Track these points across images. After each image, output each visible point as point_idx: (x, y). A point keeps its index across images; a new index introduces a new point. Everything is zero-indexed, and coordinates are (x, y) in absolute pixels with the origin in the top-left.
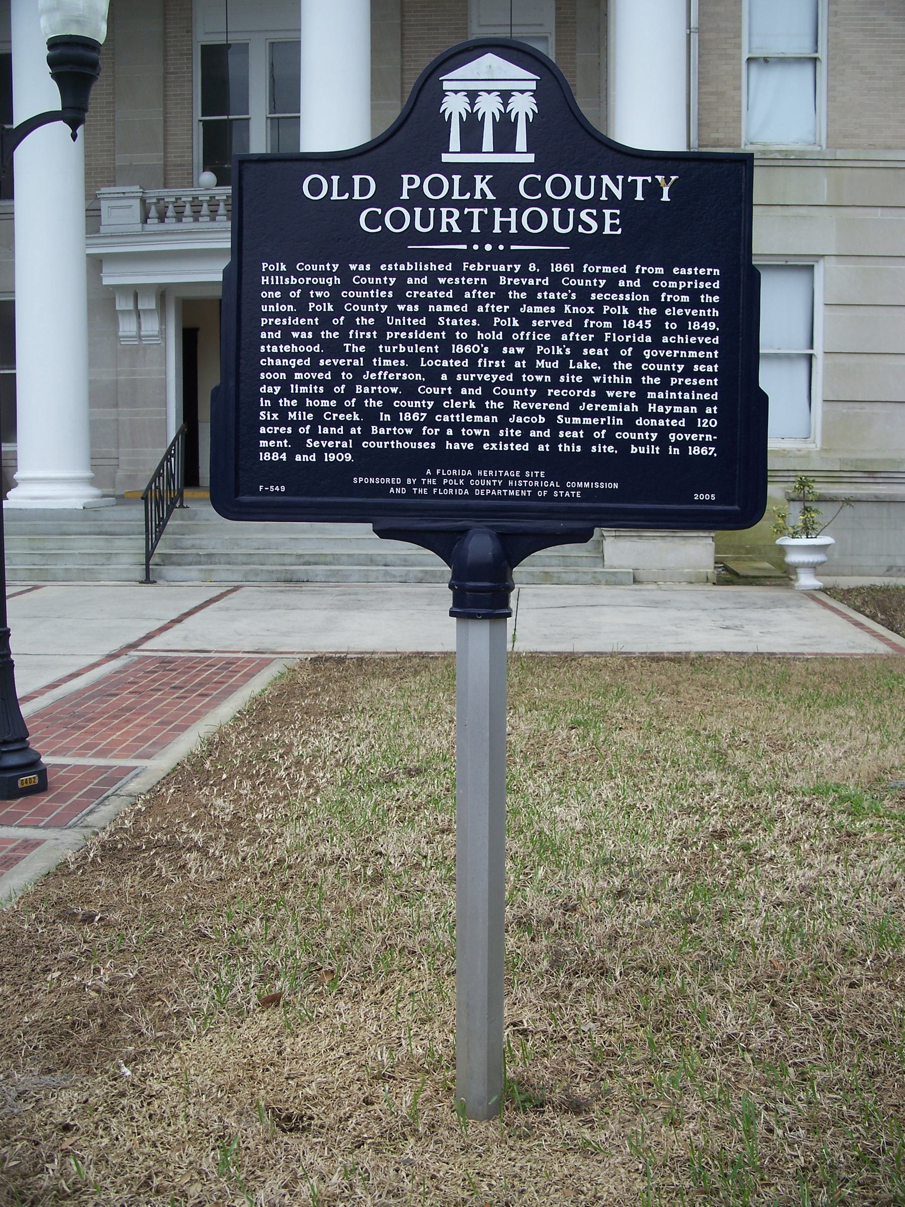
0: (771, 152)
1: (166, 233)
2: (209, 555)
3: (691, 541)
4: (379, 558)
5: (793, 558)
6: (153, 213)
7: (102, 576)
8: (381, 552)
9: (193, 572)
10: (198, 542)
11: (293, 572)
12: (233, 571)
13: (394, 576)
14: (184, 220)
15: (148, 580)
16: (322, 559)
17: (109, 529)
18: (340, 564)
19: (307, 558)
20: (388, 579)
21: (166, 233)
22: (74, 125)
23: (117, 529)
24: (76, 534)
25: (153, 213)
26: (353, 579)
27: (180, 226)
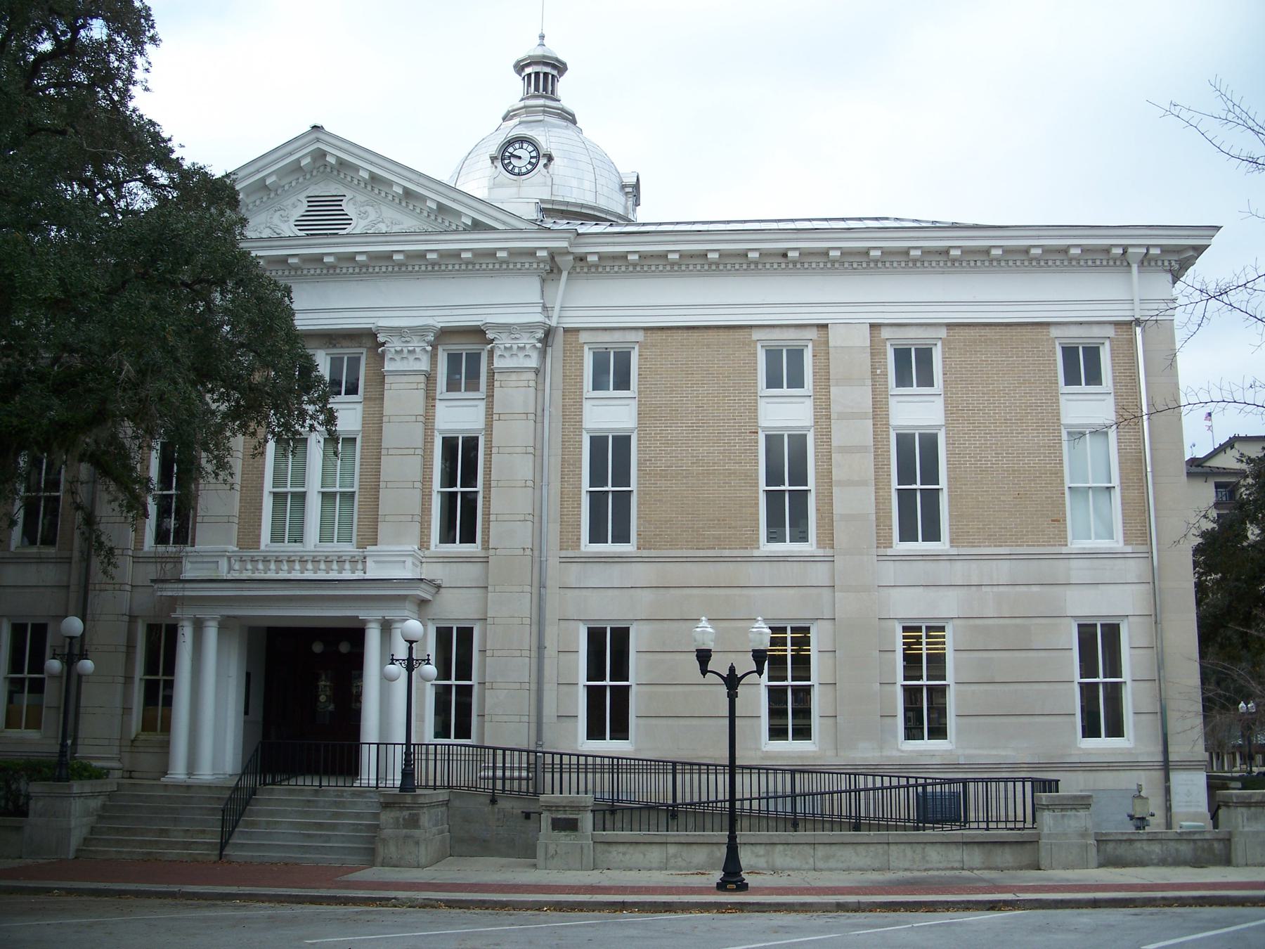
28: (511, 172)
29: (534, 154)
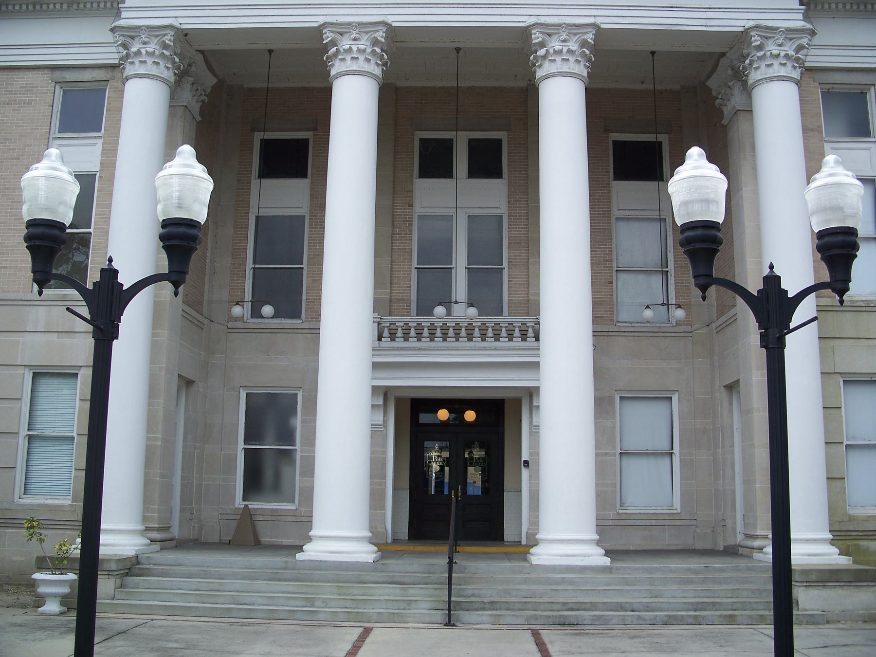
0: (857, 301)
1: (394, 349)
2: (492, 603)
3: (863, 589)
4: (627, 605)
5: (42, 590)
6: (386, 333)
7: (409, 619)
8: (605, 600)
9: (485, 615)
10: (477, 592)
11: (565, 617)
12: (517, 616)
13: (645, 620)
14: (423, 339)
15: (449, 623)
16: (583, 606)
17: (399, 580)
18: (596, 610)
19: (570, 606)
20: (641, 622)
21: (394, 349)
22: (176, 285)
23: (406, 580)
24: (371, 583)
25: (386, 333)
26: (614, 622)
27: (406, 344)
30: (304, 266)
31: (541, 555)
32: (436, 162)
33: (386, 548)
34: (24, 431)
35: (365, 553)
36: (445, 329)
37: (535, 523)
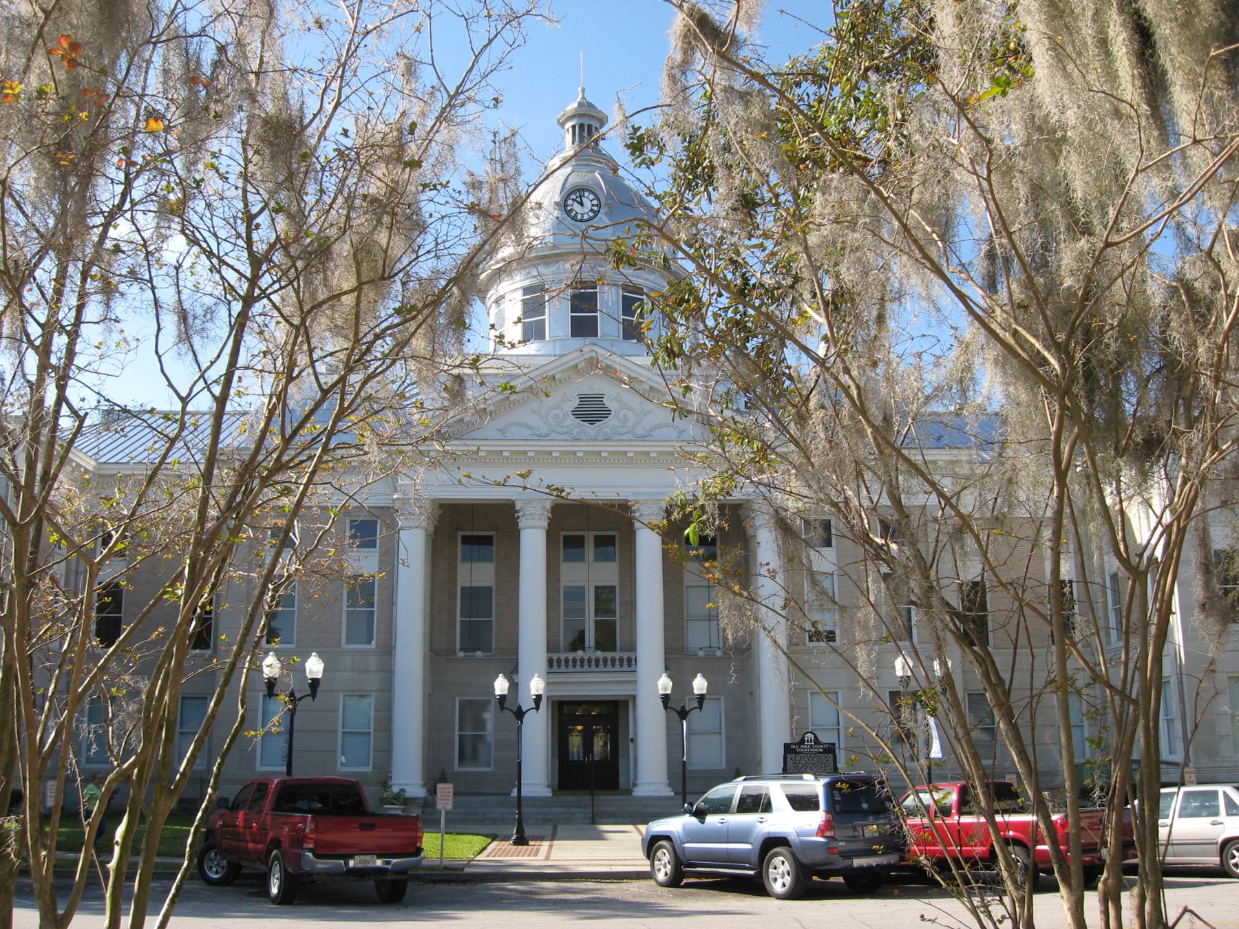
28: (574, 218)
29: (595, 202)
30: (493, 619)
31: (638, 792)
32: (574, 543)
33: (554, 792)
34: (340, 730)
35: (548, 793)
36: (582, 660)
37: (636, 777)
